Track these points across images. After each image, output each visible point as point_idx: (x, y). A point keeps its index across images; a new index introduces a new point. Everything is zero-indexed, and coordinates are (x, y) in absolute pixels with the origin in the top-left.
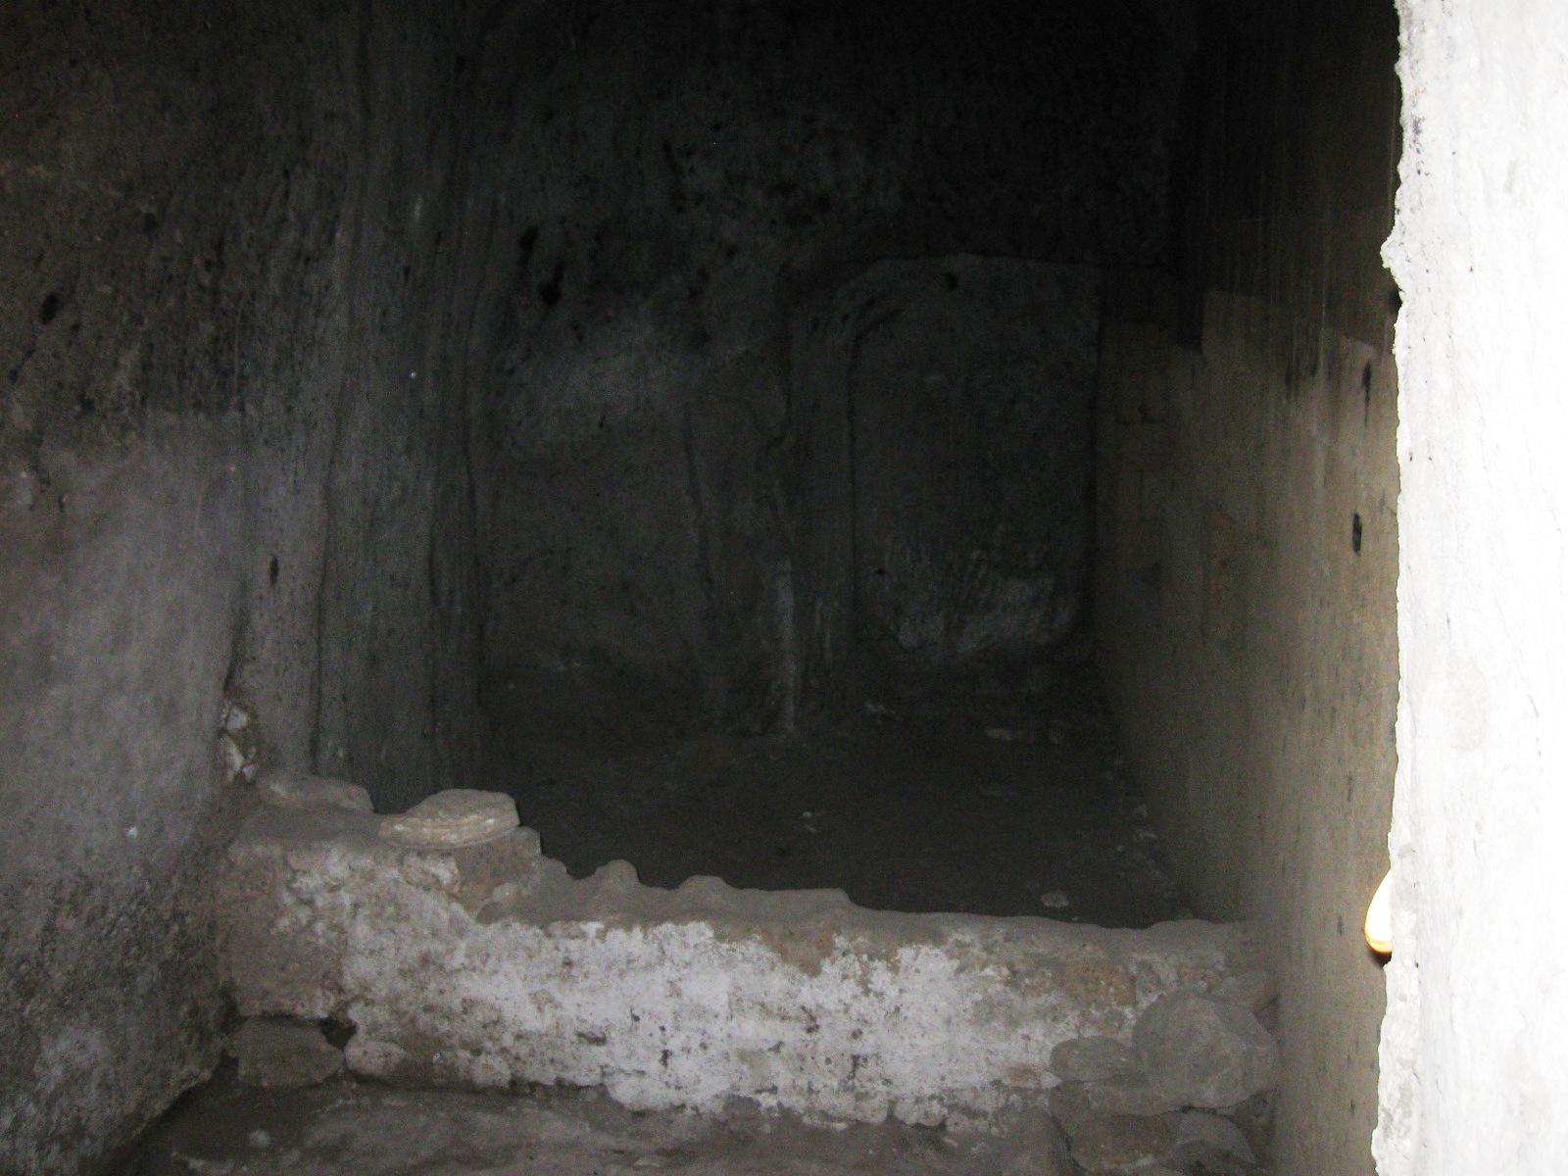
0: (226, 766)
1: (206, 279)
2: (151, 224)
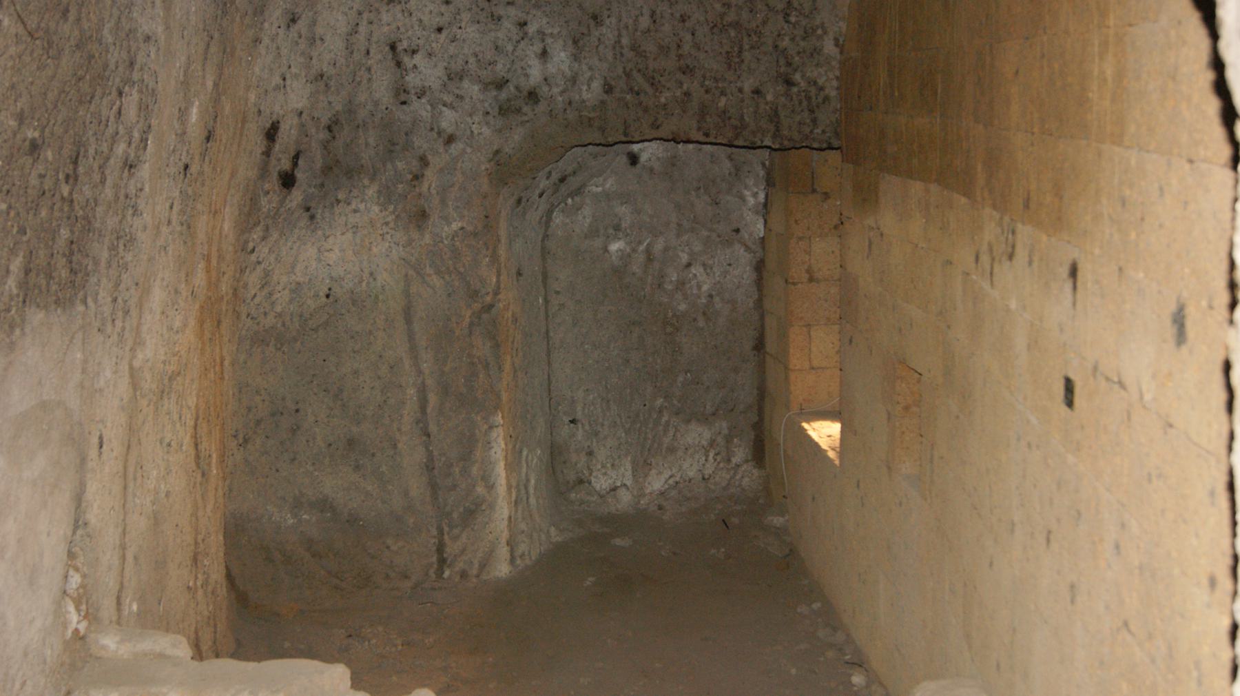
0: (65, 625)
1: (65, 190)
2: (35, 147)
